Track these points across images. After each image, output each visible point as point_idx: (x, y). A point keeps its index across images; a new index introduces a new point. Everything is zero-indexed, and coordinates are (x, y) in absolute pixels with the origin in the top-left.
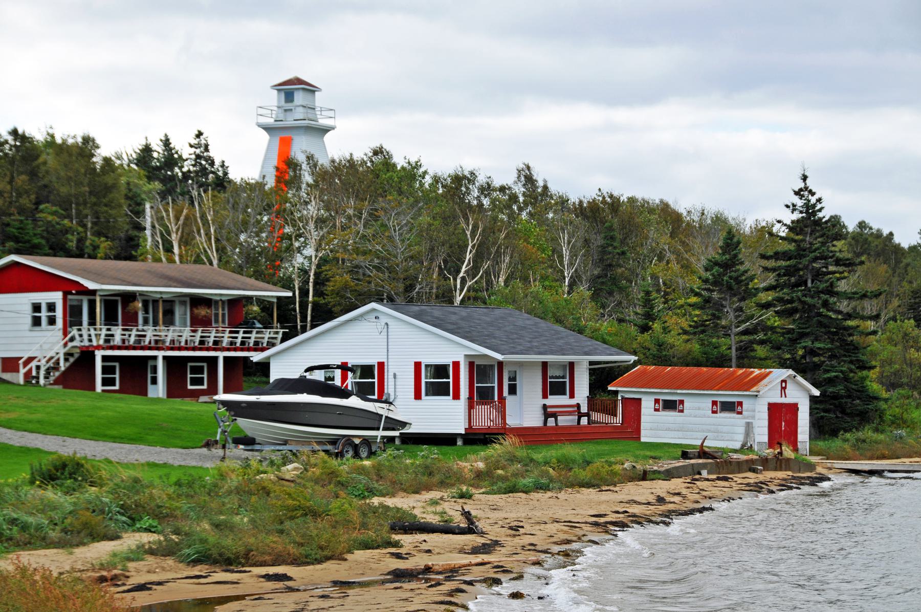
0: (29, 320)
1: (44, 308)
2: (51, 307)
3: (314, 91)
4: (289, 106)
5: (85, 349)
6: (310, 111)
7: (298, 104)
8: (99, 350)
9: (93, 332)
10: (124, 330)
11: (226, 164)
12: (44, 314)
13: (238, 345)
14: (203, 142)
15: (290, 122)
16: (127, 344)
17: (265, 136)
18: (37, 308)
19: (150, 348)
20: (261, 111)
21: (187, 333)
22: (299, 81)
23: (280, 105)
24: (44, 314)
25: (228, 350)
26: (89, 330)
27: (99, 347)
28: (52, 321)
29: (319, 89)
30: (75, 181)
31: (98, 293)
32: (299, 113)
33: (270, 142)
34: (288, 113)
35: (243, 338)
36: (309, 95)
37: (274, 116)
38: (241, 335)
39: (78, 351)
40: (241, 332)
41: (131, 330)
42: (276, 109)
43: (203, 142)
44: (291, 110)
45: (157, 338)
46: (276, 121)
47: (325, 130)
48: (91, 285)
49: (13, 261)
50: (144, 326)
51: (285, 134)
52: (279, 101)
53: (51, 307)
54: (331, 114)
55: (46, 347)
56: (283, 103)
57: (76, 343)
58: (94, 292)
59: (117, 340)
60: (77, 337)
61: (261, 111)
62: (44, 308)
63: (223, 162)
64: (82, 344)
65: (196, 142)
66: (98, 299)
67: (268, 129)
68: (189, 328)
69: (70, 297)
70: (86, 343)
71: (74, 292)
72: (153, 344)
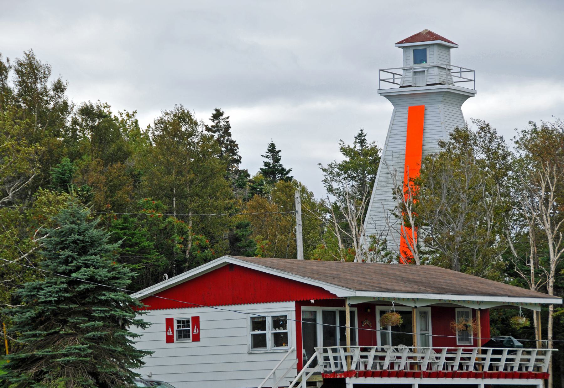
0: (249, 341)
1: (269, 323)
2: (279, 322)
3: (449, 48)
4: (420, 67)
5: (329, 376)
6: (444, 72)
7: (432, 64)
8: (350, 377)
9: (330, 354)
10: (363, 350)
11: (277, 149)
12: (269, 332)
13: (516, 369)
14: (222, 123)
15: (421, 87)
16: (396, 368)
17: (389, 106)
18: (169, 322)
19: (406, 375)
20: (384, 75)
21: (430, 355)
22: (431, 36)
23: (408, 67)
24: (269, 332)
25: (491, 376)
26: (325, 351)
27: (350, 374)
28: (280, 340)
29: (455, 46)
30: (363, 154)
31: (347, 303)
32: (434, 76)
33: (395, 113)
34: (419, 76)
35: (522, 360)
36: (443, 52)
37: (397, 81)
38: (505, 356)
39: (321, 378)
40: (505, 353)
41: (403, 350)
42: (401, 72)
43: (222, 123)
44: (424, 71)
45: (412, 361)
46: (401, 87)
47: (464, 96)
48: (340, 292)
49: (225, 262)
50: (382, 345)
51: (416, 103)
52: (406, 60)
53: (279, 322)
54: (470, 76)
55: (279, 374)
56: (411, 63)
57: (319, 368)
58: (341, 302)
59: (501, 365)
60: (321, 361)
61: (384, 75)
62: (269, 323)
63: (273, 145)
64: (328, 369)
65: (214, 124)
66: (348, 310)
67: (391, 97)
68: (431, 347)
69: (303, 308)
70: (333, 369)
71: (312, 301)
72: (408, 370)
